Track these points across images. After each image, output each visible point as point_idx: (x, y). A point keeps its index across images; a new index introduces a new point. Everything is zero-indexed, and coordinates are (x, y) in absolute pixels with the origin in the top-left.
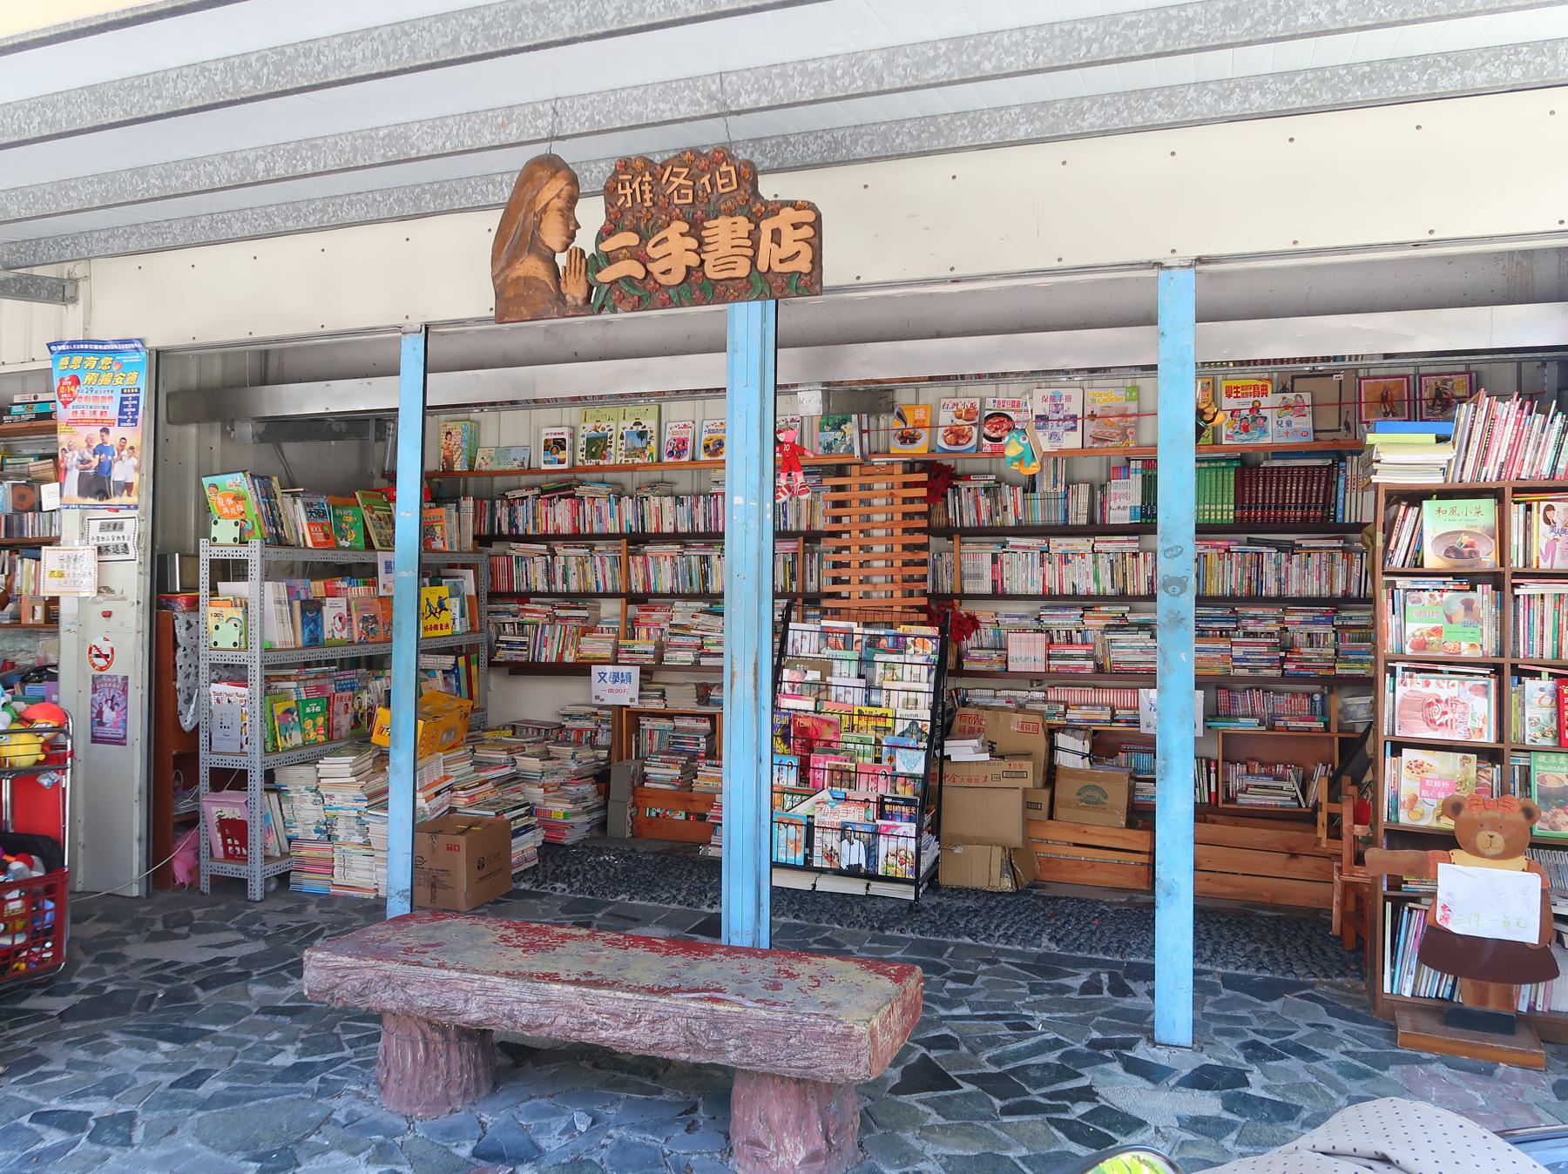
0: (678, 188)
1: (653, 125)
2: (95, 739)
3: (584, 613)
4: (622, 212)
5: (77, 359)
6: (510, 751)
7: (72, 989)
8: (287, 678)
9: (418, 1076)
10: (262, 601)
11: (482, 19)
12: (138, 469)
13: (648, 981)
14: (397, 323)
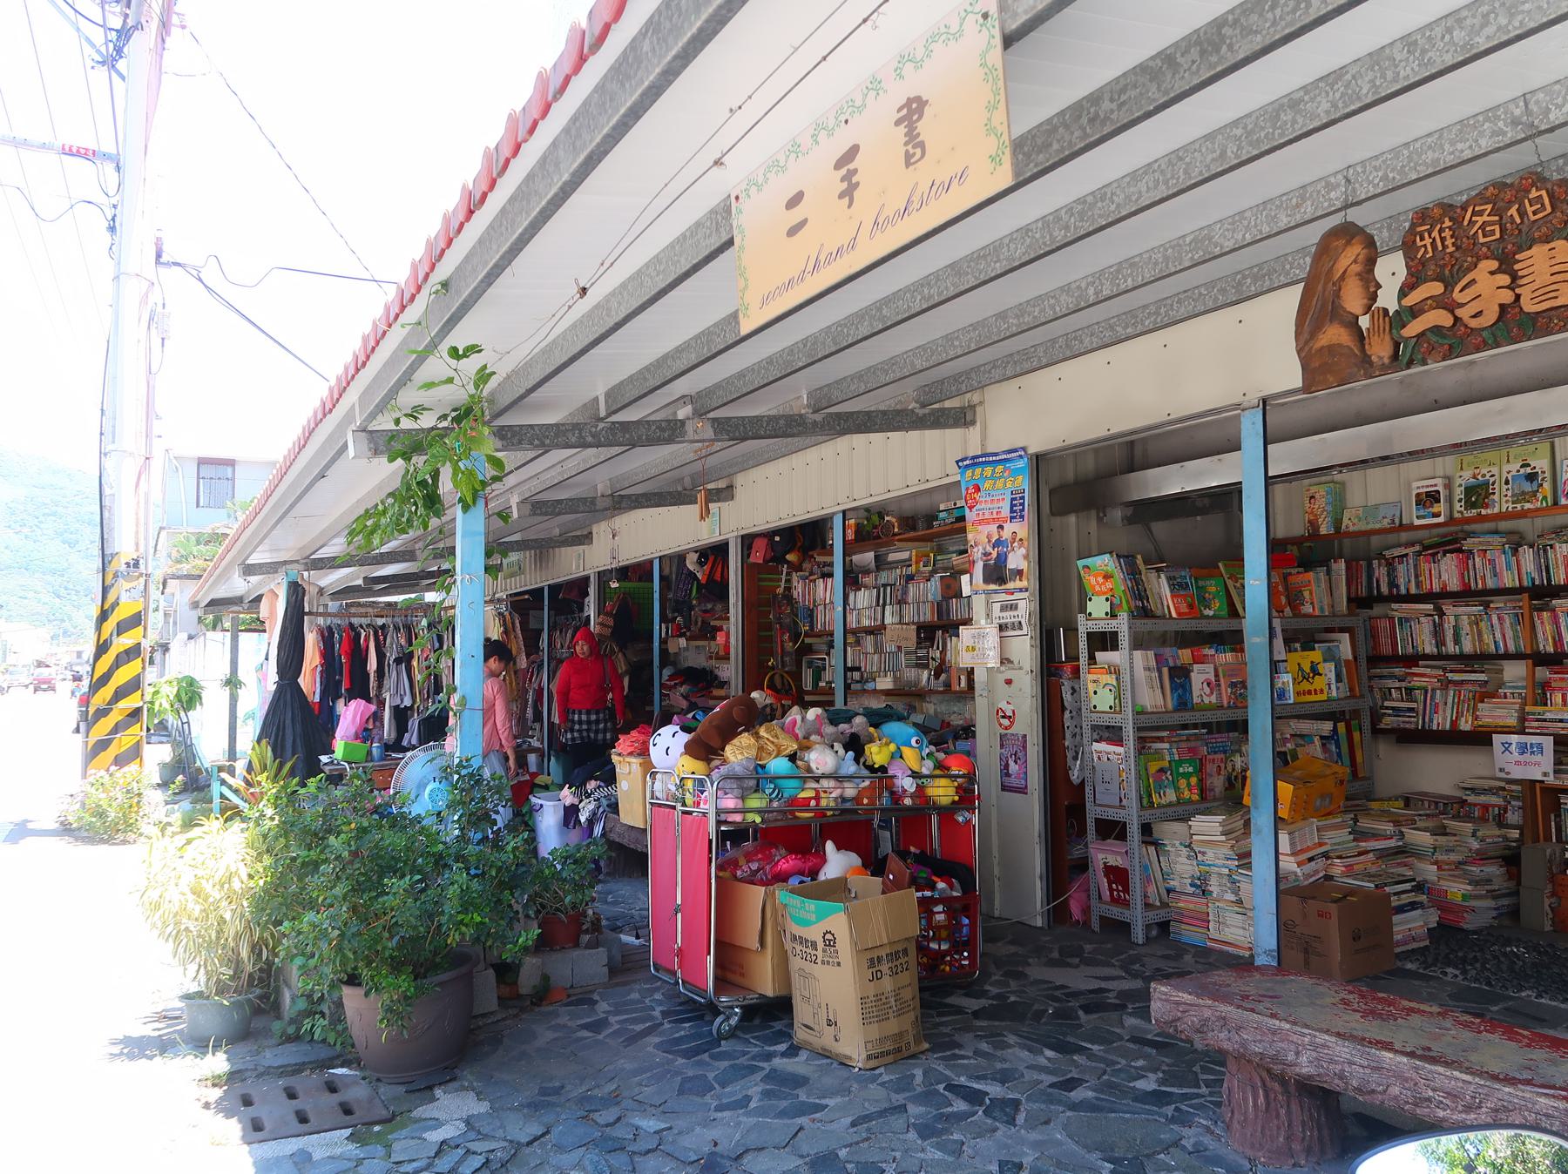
0: (1483, 227)
1: (1452, 167)
2: (1004, 788)
3: (1483, 677)
4: (1423, 263)
5: (978, 470)
6: (1397, 823)
7: (983, 994)
8: (1161, 739)
9: (1260, 1123)
10: (1132, 668)
11: (1245, 127)
12: (1026, 557)
13: (1495, 1068)
14: (1236, 401)
